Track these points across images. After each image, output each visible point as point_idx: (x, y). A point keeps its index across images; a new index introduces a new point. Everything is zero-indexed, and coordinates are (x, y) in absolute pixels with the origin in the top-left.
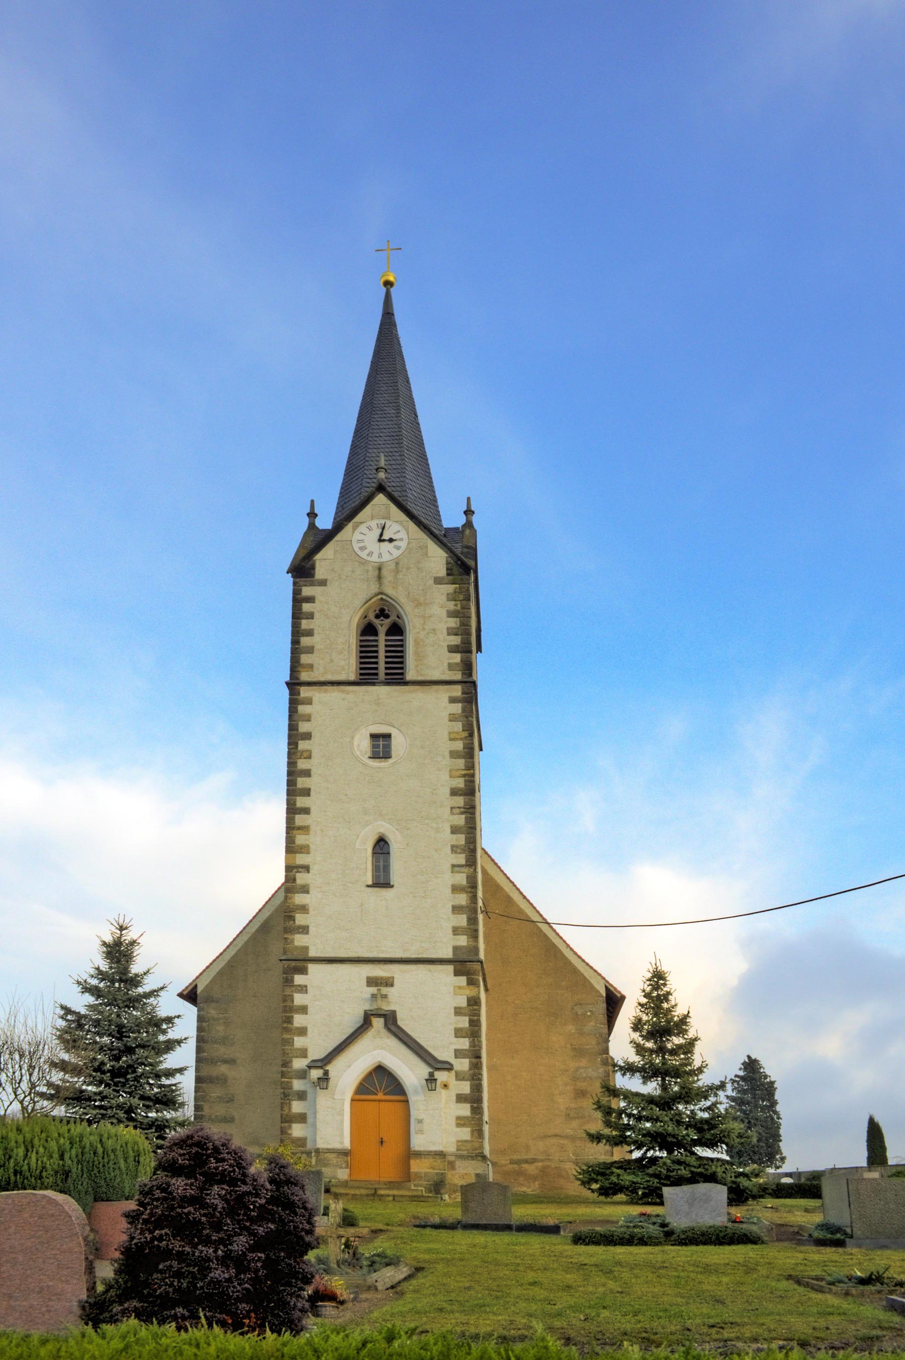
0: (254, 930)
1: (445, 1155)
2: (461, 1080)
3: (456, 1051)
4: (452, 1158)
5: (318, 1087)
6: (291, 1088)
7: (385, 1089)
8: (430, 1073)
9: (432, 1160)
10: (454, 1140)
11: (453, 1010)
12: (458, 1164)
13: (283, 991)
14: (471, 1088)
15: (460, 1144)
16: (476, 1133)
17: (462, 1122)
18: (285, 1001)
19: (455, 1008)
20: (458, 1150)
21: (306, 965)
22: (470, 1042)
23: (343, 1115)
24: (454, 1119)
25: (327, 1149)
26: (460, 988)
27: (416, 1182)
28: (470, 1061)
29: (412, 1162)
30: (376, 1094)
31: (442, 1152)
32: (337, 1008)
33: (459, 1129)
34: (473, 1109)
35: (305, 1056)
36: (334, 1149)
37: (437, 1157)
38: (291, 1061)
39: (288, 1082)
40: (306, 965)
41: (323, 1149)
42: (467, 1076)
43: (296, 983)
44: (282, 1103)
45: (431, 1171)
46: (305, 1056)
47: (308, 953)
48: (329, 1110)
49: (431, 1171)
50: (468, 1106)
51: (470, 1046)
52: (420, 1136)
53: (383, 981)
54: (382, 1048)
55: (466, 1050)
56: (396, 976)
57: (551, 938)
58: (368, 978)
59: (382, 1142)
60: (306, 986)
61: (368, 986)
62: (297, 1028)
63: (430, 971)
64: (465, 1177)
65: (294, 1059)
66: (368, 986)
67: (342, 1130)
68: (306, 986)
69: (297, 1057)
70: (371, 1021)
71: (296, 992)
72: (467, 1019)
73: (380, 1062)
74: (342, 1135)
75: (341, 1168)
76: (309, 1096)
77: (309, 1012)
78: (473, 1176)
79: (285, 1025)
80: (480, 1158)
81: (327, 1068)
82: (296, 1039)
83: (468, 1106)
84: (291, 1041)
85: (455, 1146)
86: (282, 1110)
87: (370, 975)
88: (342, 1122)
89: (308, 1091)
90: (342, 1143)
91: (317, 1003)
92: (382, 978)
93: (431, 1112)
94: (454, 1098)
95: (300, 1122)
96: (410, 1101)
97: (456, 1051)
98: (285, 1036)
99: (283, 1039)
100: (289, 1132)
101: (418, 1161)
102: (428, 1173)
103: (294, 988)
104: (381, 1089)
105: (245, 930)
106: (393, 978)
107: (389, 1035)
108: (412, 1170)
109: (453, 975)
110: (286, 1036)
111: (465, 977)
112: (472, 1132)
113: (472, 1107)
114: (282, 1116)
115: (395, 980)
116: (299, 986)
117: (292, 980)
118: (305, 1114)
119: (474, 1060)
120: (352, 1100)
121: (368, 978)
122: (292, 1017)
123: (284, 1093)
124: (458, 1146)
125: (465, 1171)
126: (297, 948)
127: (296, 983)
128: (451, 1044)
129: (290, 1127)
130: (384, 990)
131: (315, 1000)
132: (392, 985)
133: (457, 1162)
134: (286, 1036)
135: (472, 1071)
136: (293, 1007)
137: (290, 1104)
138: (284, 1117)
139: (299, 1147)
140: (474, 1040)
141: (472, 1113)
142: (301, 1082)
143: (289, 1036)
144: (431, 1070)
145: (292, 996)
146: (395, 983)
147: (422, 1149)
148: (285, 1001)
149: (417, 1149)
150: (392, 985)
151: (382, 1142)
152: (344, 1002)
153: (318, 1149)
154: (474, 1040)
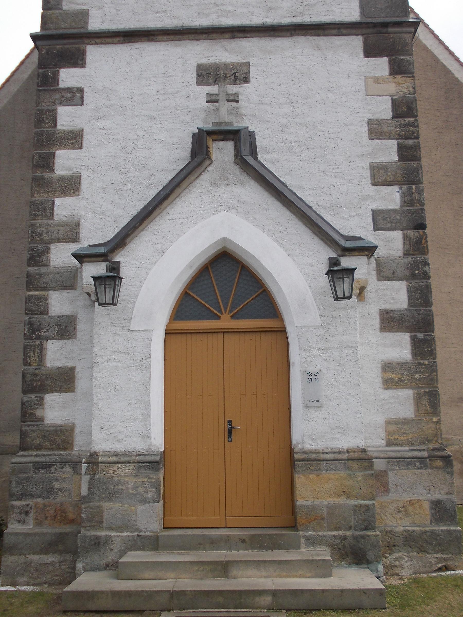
0: (26, 76)
1: (370, 460)
2: (388, 279)
3: (376, 214)
4: (379, 465)
5: (96, 304)
6: (45, 312)
7: (232, 308)
8: (330, 259)
9: (343, 474)
10: (380, 420)
11: (365, 128)
12: (392, 478)
13: (38, 104)
14: (410, 297)
15: (393, 428)
16: (425, 402)
17: (395, 377)
18: (39, 121)
19: (370, 122)
20: (389, 444)
21: (83, 47)
22: (403, 195)
23: (148, 368)
24: (379, 370)
25: (115, 454)
26: (377, 80)
27: (310, 533)
28: (405, 237)
29: (299, 479)
30: (219, 318)
31: (364, 451)
32: (141, 133)
33: (389, 393)
34: (415, 342)
35: (75, 239)
36: (128, 454)
37: (356, 465)
38: (47, 251)
39: (39, 298)
40: (83, 47)
41: (106, 454)
42: (400, 271)
43: (62, 85)
44: (25, 348)
45: (342, 501)
46: (75, 239)
47: (87, 23)
48: (120, 357)
49: (342, 501)
50: (405, 337)
51: (404, 203)
52: (314, 414)
53: (229, 73)
54: (230, 208)
55: (394, 211)
56: (253, 61)
57: (453, 71)
58: (200, 67)
59: (230, 431)
60: (81, 90)
61: (199, 83)
62: (62, 179)
63: (318, 48)
64: (410, 509)
65: (52, 246)
66: (199, 83)
67: (148, 406)
68: (81, 90)
69: (59, 241)
70: (207, 147)
71: (61, 104)
72: (393, 144)
73: (224, 239)
74: (146, 417)
75: (144, 501)
76: (80, 327)
77: (84, 145)
78: (426, 506)
79: (38, 174)
80: (439, 463)
81: (116, 259)
82: (58, 201)
83: (405, 337)
84: (49, 205)
85: (383, 434)
86: (26, 363)
87: (204, 61)
88: (147, 386)
89: (80, 317)
90: (145, 437)
91: (101, 123)
92: (226, 65)
93: (336, 353)
94: (376, 322)
95: (60, 390)
96: (289, 329)
97: (376, 214)
98: (37, 198)
99: (33, 203)
100: (39, 413)
101: (312, 477)
102: (336, 506)
103: (58, 96)
104: (220, 311)
105: (15, 77)
106: (248, 64)
107: (245, 177)
108: (300, 502)
109: (362, 55)
110: (40, 197)
111: (385, 59)
112: (418, 399)
113: (414, 339)
114: (24, 376)
115: (252, 69)
116: (69, 90)
117: (55, 79)
118: (72, 369)
119: (413, 234)
120: (168, 333)
121: (200, 67)
122: (53, 154)
123: (31, 324)
124: (388, 433)
125: (407, 497)
126: (67, 14)
127: (62, 85)
128: (365, 199)
129: (40, 402)
130: (232, 89)
131: (98, 119)
132: (246, 80)
133: (391, 475)
134: (40, 197)
135: (409, 259)
136: (54, 134)
137: (42, 348)
138: (29, 378)
139: (58, 448)
140: (410, 189)
141: (415, 354)
142: (65, 294)
143: (44, 198)
144: (334, 255)
145: (54, 111)
146: (252, 75)
147: (319, 445)
148: (39, 121)
149: (309, 445)
150: (246, 80)
151: (230, 431)
152: (152, 118)
153: (94, 455)
154: (410, 189)
